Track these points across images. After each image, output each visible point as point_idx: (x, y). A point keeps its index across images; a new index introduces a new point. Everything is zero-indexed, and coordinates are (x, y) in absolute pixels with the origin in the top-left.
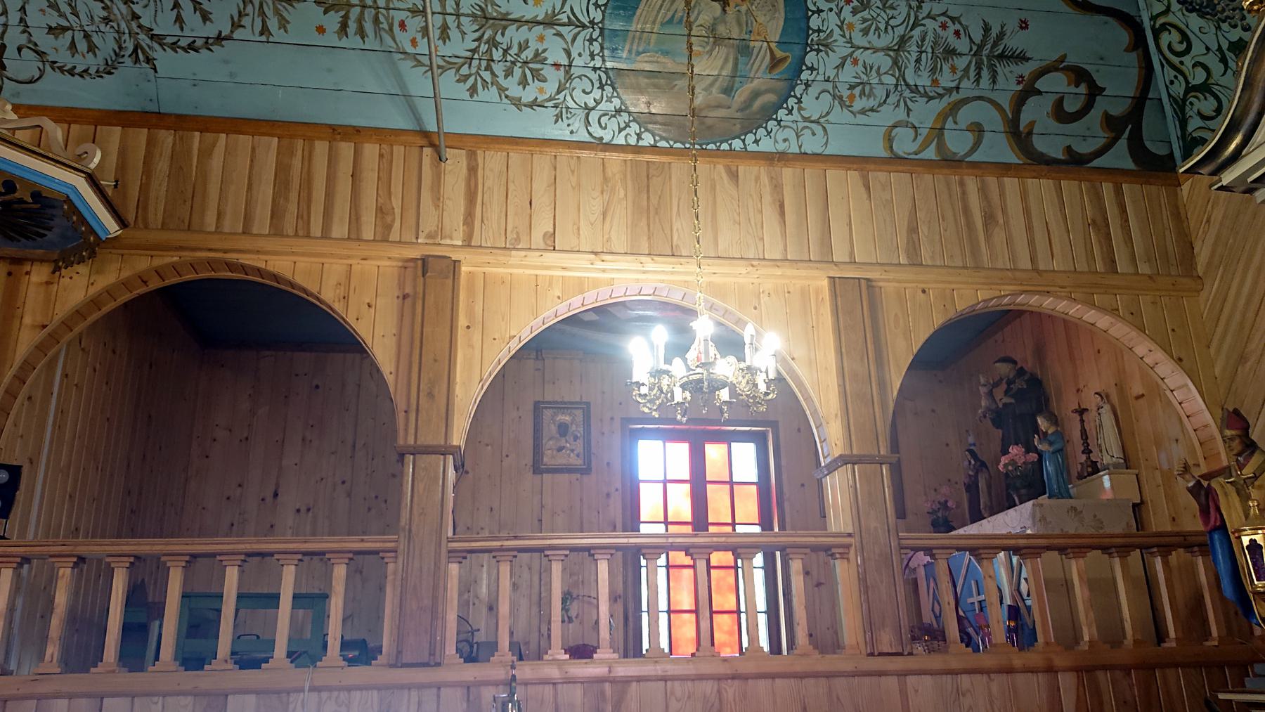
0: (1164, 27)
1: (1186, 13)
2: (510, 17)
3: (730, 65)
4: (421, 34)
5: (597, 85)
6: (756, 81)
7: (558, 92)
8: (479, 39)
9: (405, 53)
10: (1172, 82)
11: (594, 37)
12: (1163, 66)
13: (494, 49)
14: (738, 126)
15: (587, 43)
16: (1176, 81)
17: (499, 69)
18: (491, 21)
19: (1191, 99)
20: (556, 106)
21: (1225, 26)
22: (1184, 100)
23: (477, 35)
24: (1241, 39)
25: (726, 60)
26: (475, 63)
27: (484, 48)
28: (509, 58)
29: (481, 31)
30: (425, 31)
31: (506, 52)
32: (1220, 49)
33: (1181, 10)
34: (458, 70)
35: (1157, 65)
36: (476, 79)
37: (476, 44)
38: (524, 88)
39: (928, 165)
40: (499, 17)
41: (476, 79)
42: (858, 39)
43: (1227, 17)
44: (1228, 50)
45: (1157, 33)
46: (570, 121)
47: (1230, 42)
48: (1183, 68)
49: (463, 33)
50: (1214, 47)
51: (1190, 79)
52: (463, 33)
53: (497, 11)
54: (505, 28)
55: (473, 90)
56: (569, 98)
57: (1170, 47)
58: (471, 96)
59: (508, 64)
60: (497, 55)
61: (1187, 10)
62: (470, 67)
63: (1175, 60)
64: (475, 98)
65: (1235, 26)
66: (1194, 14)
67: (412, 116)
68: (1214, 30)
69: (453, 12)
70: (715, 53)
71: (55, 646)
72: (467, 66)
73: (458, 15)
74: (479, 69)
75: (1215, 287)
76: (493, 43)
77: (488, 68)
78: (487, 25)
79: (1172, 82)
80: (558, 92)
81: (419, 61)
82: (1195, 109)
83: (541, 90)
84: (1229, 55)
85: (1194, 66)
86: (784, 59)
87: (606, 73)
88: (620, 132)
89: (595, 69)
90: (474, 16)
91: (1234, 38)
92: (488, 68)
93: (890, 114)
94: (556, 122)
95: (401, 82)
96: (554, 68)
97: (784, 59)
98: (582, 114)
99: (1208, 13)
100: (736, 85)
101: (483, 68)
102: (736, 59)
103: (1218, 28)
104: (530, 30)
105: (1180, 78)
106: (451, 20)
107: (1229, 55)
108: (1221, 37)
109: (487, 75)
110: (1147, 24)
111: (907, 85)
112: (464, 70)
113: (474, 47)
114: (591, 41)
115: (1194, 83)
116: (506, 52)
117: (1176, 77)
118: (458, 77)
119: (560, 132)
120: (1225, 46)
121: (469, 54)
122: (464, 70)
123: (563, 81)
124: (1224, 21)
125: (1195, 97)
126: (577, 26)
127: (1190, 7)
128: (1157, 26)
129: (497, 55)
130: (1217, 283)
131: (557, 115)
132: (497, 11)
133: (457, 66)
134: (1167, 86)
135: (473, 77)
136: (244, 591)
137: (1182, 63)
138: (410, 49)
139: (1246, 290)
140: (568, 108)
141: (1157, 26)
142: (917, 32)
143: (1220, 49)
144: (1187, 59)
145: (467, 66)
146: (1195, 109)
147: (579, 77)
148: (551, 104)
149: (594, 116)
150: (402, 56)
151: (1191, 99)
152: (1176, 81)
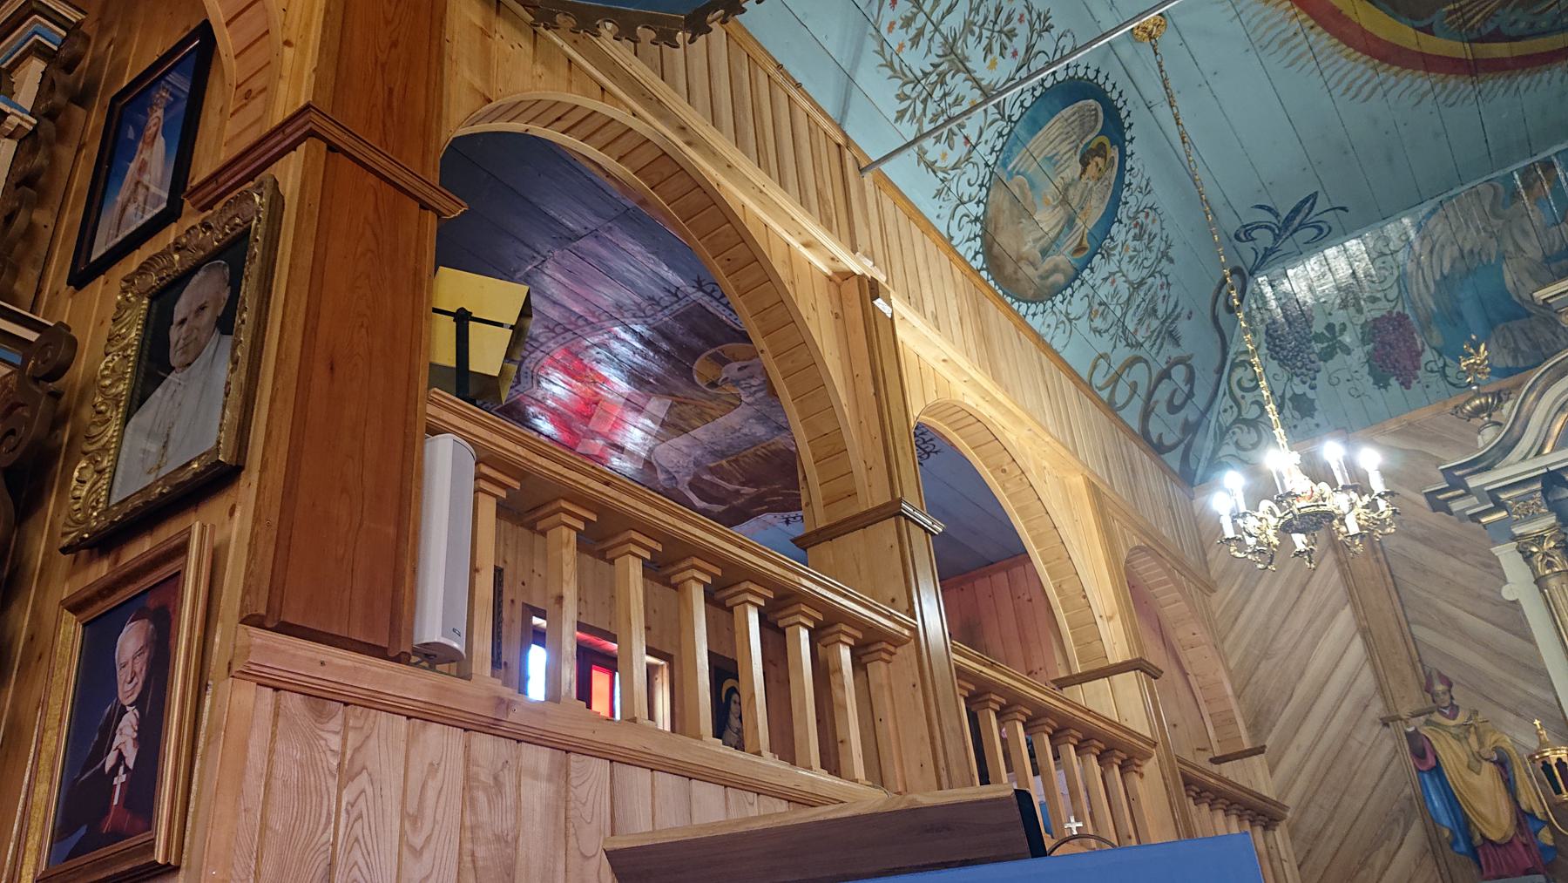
0: (1243, 364)
1: (1268, 357)
2: (967, 64)
3: (1057, 230)
4: (901, 22)
5: (979, 182)
6: (1062, 257)
7: (954, 168)
8: (935, 66)
9: (878, 31)
10: (1225, 411)
11: (1004, 133)
12: (1225, 394)
13: (939, 86)
14: (1032, 292)
15: (996, 135)
16: (1230, 410)
17: (932, 108)
18: (953, 56)
19: (1236, 430)
20: (943, 181)
21: (1296, 380)
22: (1228, 429)
23: (937, 60)
24: (1304, 394)
25: (1057, 224)
26: (919, 87)
27: (933, 78)
28: (943, 105)
29: (942, 60)
30: (907, 22)
31: (945, 95)
32: (1282, 397)
33: (1266, 355)
34: (905, 84)
35: (1221, 393)
36: (910, 106)
37: (931, 69)
38: (936, 143)
39: (1097, 401)
40: (961, 57)
41: (910, 106)
42: (1124, 266)
43: (1302, 374)
44: (1290, 399)
45: (1234, 366)
46: (944, 204)
47: (1294, 393)
48: (1242, 402)
49: (929, 51)
50: (1279, 393)
51: (1243, 413)
52: (929, 51)
53: (962, 50)
54: (958, 71)
55: (901, 115)
56: (956, 179)
57: (1239, 382)
58: (896, 120)
59: (940, 109)
60: (938, 94)
61: (1271, 357)
62: (913, 89)
63: (1238, 393)
64: (897, 125)
65: (1304, 383)
66: (1276, 362)
67: (842, 105)
68: (1285, 379)
69: (935, 22)
70: (1057, 210)
71: (613, 455)
72: (912, 85)
73: (936, 29)
74: (918, 96)
75: (1232, 592)
76: (942, 76)
77: (924, 102)
78: (948, 58)
79: (1225, 411)
80: (954, 168)
81: (883, 50)
82: (1235, 439)
83: (945, 155)
84: (1288, 404)
85: (1253, 403)
86: (1085, 249)
87: (991, 173)
88: (967, 241)
89: (987, 165)
90: (946, 39)
91: (1299, 391)
92: (924, 102)
93: (1103, 344)
94: (935, 197)
95: (856, 60)
96: (963, 140)
97: (1085, 249)
98: (955, 201)
99: (1288, 365)
100: (1051, 251)
101: (921, 98)
102: (1063, 227)
103: (1290, 379)
104: (972, 88)
105: (1235, 409)
106: (930, 27)
107: (1288, 404)
108: (1288, 387)
109: (920, 106)
110: (1231, 356)
111: (1123, 324)
112: (908, 89)
113: (927, 71)
114: (1000, 135)
115: (1245, 416)
116: (945, 95)
117: (1231, 407)
118: (899, 92)
119: (929, 208)
120: (1288, 395)
121: (920, 74)
122: (908, 89)
123: (962, 159)
124: (1297, 376)
125: (1241, 429)
126: (999, 113)
127: (1275, 355)
128: (1237, 361)
129: (938, 94)
130: (1235, 588)
131: (938, 190)
132: (962, 50)
133: (906, 79)
134: (1219, 413)
135: (910, 101)
136: (1030, 855)
137: (1243, 397)
138: (884, 31)
139: (1271, 598)
140: (949, 189)
141: (1237, 361)
142: (1150, 281)
143: (1282, 397)
144: (1250, 397)
145: (912, 85)
146: (1235, 439)
147: (974, 164)
148: (941, 175)
149: (961, 210)
150: (874, 33)
151: (1236, 430)
152: (1230, 410)
